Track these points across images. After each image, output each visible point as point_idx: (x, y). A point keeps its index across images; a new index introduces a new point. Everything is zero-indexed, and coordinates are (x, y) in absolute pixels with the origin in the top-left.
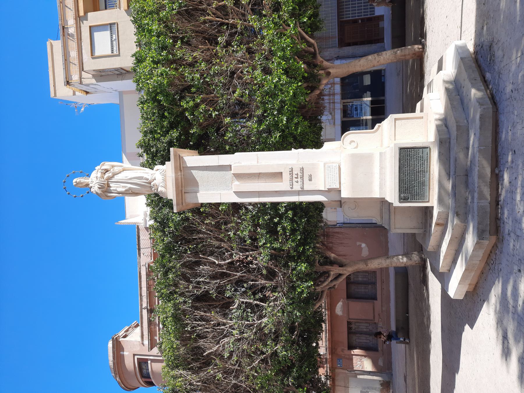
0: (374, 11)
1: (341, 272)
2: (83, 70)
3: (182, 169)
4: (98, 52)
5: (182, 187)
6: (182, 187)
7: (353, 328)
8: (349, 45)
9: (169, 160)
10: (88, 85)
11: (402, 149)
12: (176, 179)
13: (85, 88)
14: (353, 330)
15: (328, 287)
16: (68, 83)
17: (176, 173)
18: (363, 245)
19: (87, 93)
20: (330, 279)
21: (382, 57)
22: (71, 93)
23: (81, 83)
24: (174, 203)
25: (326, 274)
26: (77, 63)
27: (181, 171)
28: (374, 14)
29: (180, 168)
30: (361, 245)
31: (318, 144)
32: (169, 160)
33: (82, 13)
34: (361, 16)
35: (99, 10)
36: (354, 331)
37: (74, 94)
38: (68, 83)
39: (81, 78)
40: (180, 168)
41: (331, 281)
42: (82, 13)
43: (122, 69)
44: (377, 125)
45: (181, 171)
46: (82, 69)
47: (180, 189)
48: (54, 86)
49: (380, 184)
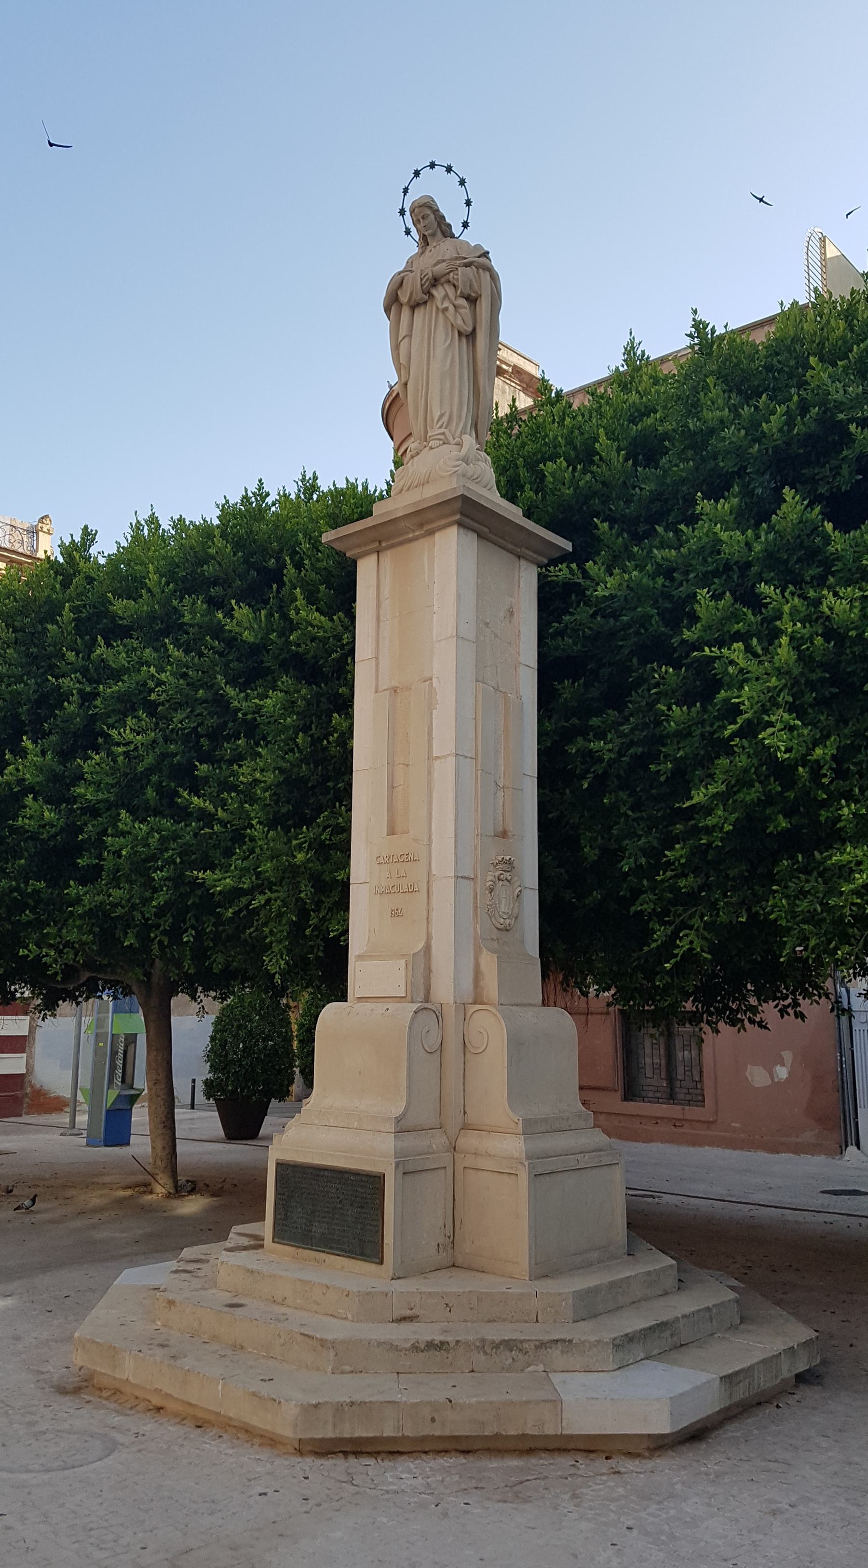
18: (782, 1073)
30: (783, 1065)
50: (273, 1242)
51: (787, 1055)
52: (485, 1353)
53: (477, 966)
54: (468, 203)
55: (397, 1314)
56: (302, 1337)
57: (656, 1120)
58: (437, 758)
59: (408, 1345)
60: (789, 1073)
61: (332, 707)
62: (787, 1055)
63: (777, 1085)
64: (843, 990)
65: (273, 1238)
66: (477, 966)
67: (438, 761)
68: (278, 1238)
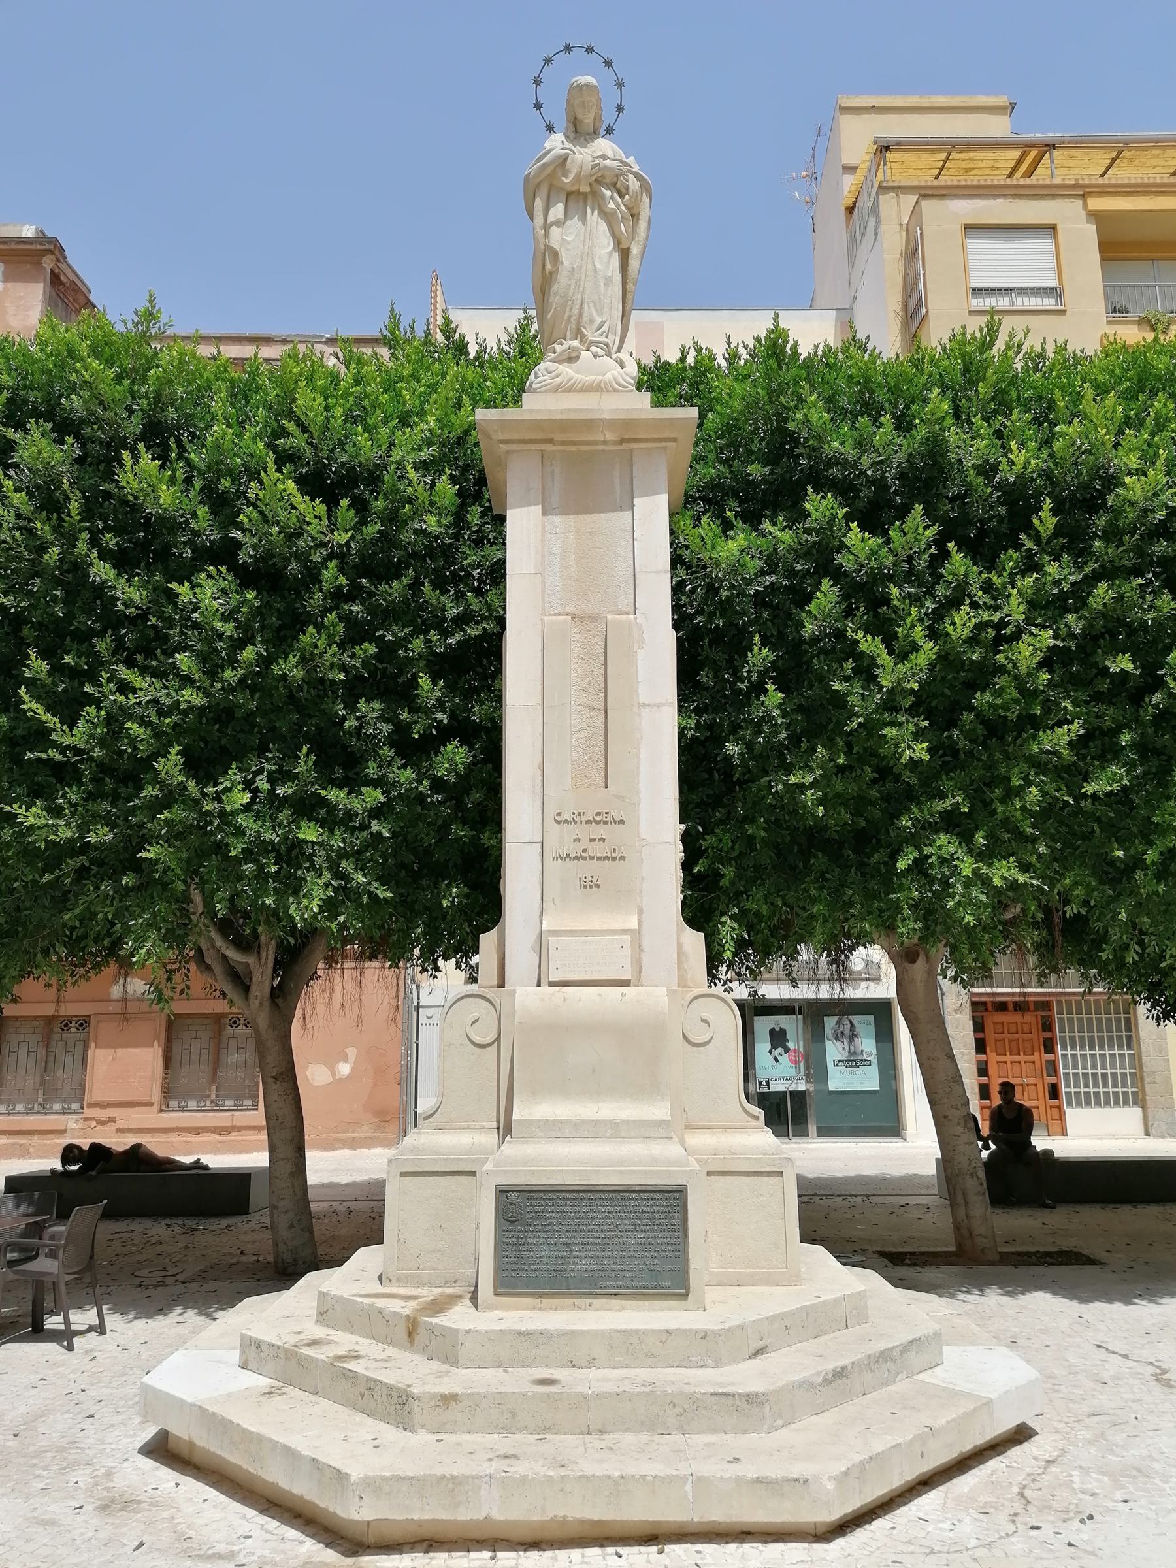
0: (1079, 1104)
1: (255, 991)
2: (925, 196)
3: (625, 446)
4: (978, 247)
5: (563, 443)
6: (563, 443)
7: (65, 1035)
8: (979, 1027)
9: (656, 404)
10: (874, 210)
11: (680, 1193)
12: (590, 424)
13: (864, 204)
14: (57, 1034)
15: (204, 948)
16: (884, 147)
17: (612, 424)
18: (344, 1069)
19: (850, 210)
20: (232, 954)
21: (960, 1129)
22: (848, 160)
23: (883, 189)
24: (510, 413)
25: (246, 944)
26: (945, 179)
27: (622, 441)
28: (1069, 1104)
29: (630, 440)
30: (346, 1061)
31: (697, 913)
32: (656, 404)
33: (1096, 203)
34: (1065, 1067)
35: (1102, 259)
36: (56, 1037)
37: (850, 169)
38: (884, 147)
39: (898, 189)
40: (630, 440)
41: (225, 957)
42: (1096, 203)
43: (923, 318)
44: (761, 1113)
45: (622, 441)
46: (926, 193)
47: (558, 437)
48: (873, 109)
49: (561, 1122)
50: (496, 1294)
51: (352, 1052)
52: (871, 1371)
53: (680, 946)
54: (548, 61)
55: (752, 1351)
56: (713, 1398)
57: (197, 1131)
58: (645, 705)
59: (820, 1380)
60: (352, 1069)
61: (22, 691)
62: (352, 1052)
63: (339, 1082)
64: (414, 986)
65: (495, 1287)
66: (680, 946)
67: (648, 709)
68: (502, 1286)
